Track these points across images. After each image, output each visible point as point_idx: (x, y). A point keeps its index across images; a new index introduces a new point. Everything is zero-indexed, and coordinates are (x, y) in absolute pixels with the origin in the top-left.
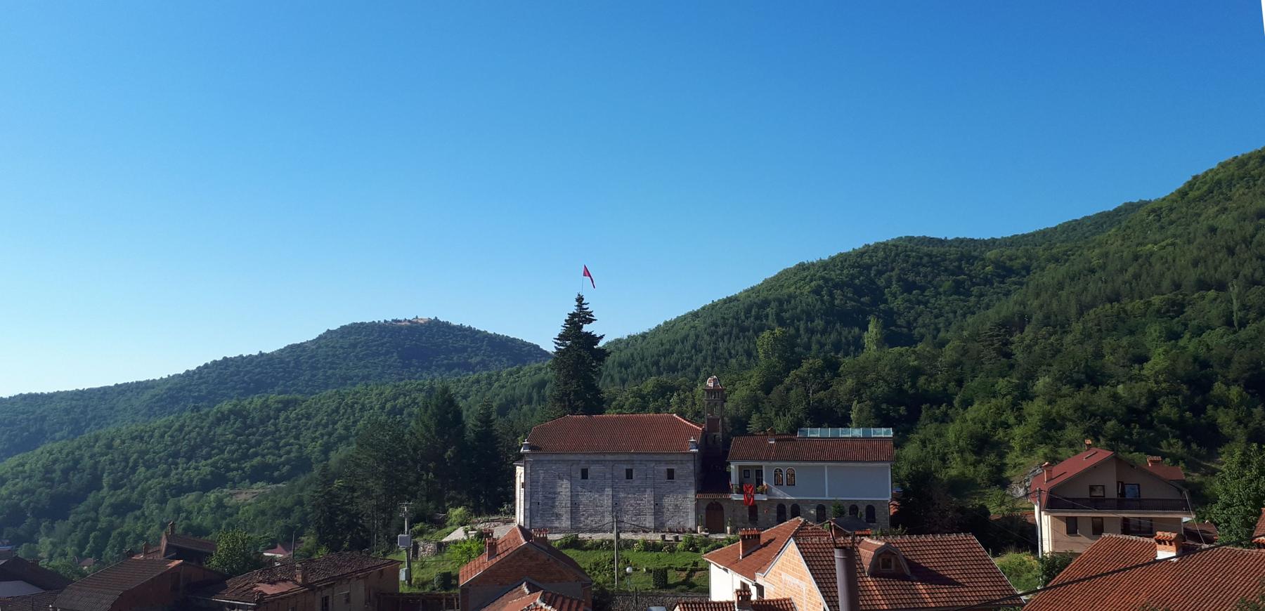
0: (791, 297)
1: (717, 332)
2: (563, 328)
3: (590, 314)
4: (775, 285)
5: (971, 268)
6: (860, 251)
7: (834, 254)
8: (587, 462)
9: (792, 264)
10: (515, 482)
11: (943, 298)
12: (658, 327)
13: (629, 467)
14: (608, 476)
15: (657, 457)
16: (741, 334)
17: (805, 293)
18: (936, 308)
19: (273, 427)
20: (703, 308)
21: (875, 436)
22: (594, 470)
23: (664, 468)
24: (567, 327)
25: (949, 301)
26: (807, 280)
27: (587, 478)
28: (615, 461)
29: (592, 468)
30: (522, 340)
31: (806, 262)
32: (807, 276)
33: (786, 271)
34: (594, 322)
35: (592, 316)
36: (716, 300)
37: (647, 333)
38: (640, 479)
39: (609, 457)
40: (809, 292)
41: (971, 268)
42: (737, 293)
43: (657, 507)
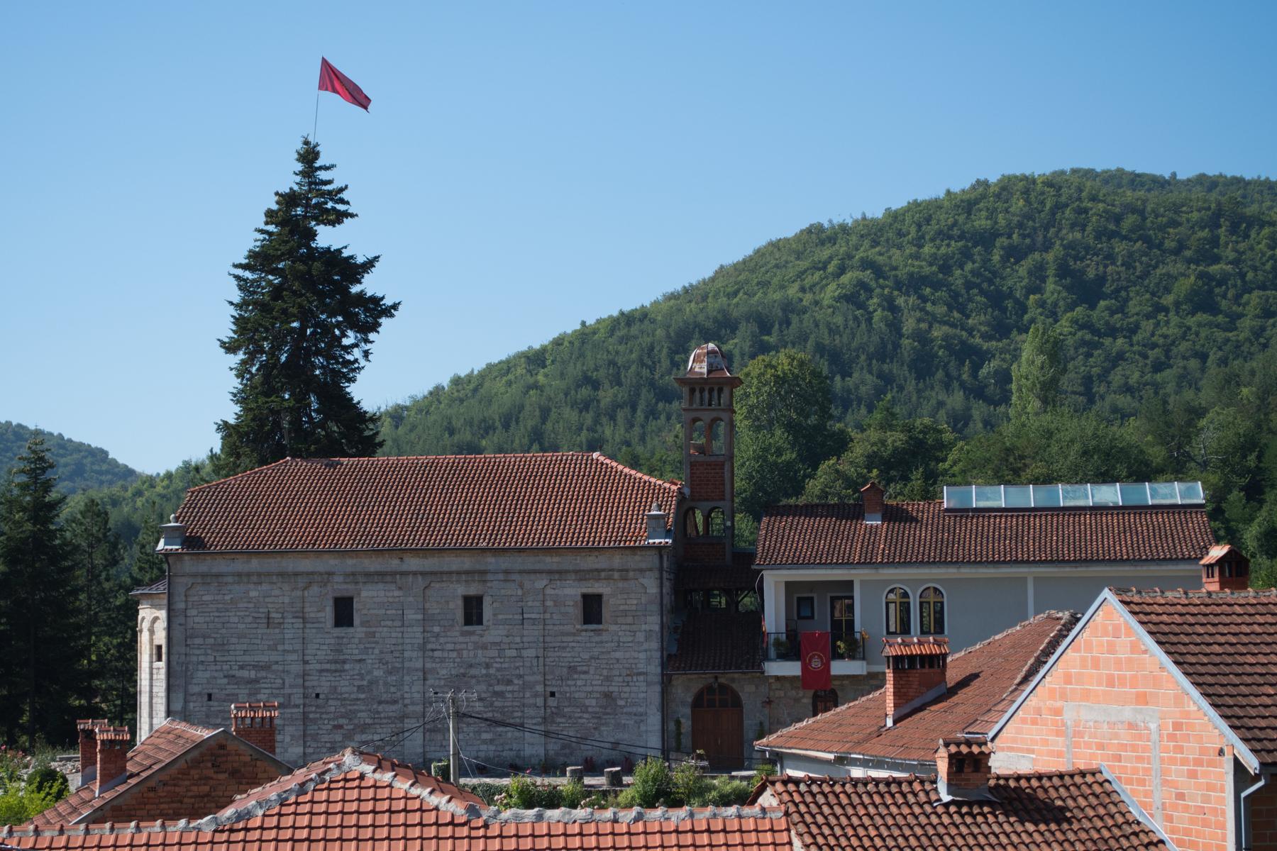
0: (789, 308)
1: (598, 401)
2: (261, 237)
3: (336, 195)
4: (747, 282)
5: (1242, 246)
6: (965, 197)
7: (898, 203)
8: (352, 576)
9: (789, 228)
10: (135, 659)
11: (1174, 319)
12: (437, 392)
13: (473, 590)
14: (411, 615)
15: (551, 562)
16: (661, 406)
17: (825, 303)
18: (1154, 346)
20: (558, 342)
21: (1157, 502)
22: (368, 599)
23: (573, 591)
24: (270, 234)
25: (1189, 328)
26: (831, 268)
27: (350, 624)
28: (432, 573)
29: (364, 594)
30: (60, 436)
31: (826, 225)
32: (831, 258)
33: (776, 246)
34: (347, 221)
35: (342, 201)
36: (591, 321)
37: (407, 408)
39: (413, 563)
40: (838, 299)
41: (1242, 246)
42: (647, 304)
43: (552, 702)
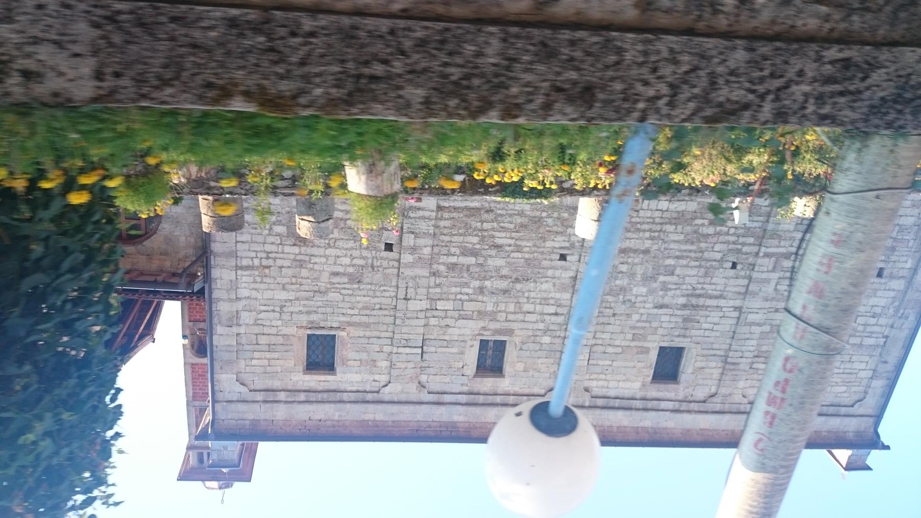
13: (488, 384)
19: (796, 138)
29: (637, 385)
38: (449, 343)
